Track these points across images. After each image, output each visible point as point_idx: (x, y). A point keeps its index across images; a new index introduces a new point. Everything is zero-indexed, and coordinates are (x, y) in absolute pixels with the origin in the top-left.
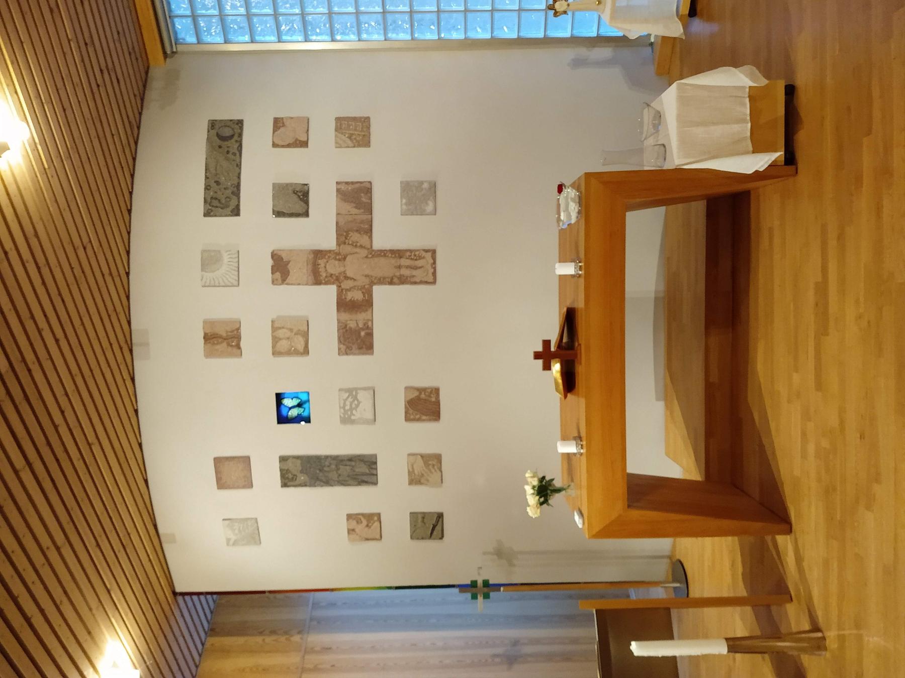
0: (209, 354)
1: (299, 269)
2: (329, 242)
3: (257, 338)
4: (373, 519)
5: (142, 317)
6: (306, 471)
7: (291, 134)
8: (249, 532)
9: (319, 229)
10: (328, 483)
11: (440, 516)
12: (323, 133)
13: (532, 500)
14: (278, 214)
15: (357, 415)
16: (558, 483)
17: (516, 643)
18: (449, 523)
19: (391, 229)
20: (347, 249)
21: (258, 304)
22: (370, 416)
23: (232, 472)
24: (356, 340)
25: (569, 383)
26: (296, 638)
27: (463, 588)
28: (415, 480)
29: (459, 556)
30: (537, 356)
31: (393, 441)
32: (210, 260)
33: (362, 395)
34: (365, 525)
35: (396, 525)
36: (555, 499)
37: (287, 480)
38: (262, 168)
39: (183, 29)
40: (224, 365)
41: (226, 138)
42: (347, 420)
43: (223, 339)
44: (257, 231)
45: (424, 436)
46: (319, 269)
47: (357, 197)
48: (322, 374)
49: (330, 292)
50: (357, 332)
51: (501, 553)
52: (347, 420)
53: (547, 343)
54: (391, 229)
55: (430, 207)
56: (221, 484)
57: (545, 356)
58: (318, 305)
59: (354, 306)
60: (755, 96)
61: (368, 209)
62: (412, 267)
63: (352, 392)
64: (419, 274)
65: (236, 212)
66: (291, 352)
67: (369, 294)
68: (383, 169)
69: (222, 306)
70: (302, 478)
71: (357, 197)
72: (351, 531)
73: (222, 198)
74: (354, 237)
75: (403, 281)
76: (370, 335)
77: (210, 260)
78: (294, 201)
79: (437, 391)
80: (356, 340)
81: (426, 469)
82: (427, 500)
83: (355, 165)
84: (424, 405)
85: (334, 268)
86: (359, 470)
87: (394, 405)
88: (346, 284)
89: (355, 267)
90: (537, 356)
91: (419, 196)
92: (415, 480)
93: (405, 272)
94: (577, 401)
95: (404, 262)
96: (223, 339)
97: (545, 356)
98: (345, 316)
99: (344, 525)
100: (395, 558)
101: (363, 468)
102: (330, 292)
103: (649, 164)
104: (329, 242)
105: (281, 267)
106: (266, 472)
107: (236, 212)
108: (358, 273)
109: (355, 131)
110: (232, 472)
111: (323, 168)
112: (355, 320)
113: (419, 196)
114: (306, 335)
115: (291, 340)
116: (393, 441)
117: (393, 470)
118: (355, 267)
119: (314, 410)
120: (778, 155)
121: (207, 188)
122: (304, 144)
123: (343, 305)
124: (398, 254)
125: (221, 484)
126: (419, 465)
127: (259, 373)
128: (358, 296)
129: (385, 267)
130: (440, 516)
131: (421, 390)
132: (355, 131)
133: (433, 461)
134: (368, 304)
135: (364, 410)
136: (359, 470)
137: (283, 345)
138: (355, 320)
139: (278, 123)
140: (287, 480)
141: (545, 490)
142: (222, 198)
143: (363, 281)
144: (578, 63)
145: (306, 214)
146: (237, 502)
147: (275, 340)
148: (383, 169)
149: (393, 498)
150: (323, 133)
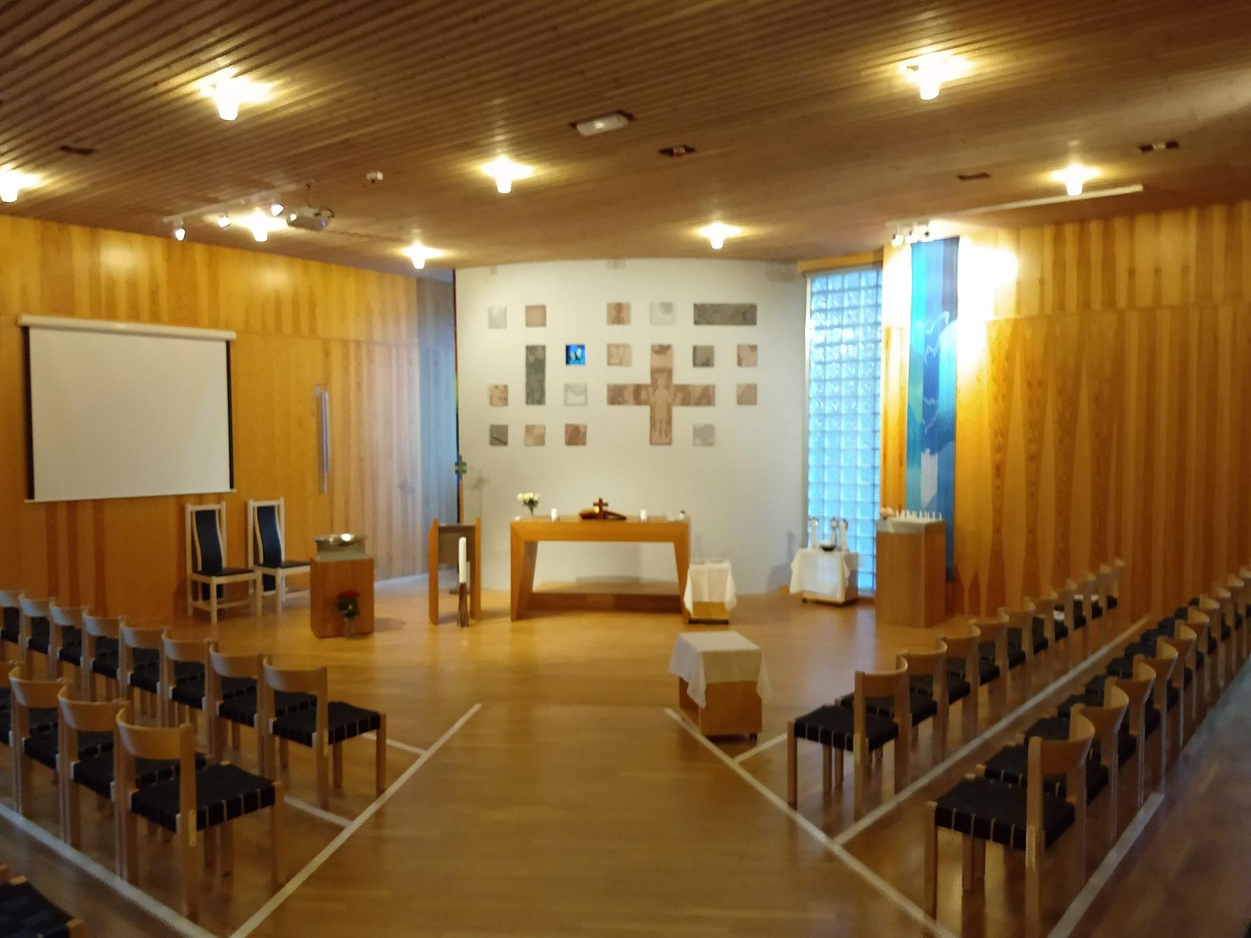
0: (609, 306)
1: (661, 361)
2: (678, 379)
3: (618, 334)
4: (504, 401)
5: (632, 265)
6: (536, 363)
7: (747, 355)
8: (497, 322)
9: (685, 373)
10: (528, 374)
11: (505, 443)
12: (747, 375)
13: (528, 496)
14: (695, 349)
15: (570, 394)
16: (535, 510)
17: (413, 491)
18: (500, 449)
19: (685, 418)
20: (673, 390)
21: (640, 335)
22: (570, 401)
23: (536, 316)
24: (616, 395)
25: (587, 516)
26: (416, 340)
27: (459, 457)
28: (529, 429)
29: (479, 454)
30: (601, 501)
31: (553, 416)
32: (667, 308)
33: (582, 398)
34: (500, 396)
35: (500, 416)
36: (527, 509)
37: (531, 349)
38: (726, 338)
39: (816, 285)
40: (603, 314)
41: (745, 315)
42: (568, 388)
43: (618, 314)
44: (685, 335)
45: (556, 436)
46: (662, 373)
47: (706, 397)
48: (596, 374)
49: (645, 379)
50: (621, 395)
51: (480, 482)
52: (568, 388)
53: (606, 505)
54: (685, 418)
55: (698, 441)
56: (529, 309)
57: (601, 504)
58: (639, 372)
59: (638, 394)
60: (721, 605)
61: (698, 403)
62: (661, 430)
63: (584, 391)
64: (656, 434)
65: (696, 323)
66: (610, 356)
67: (645, 403)
68: (723, 413)
69: (639, 312)
70: (532, 359)
71: (706, 397)
72: (497, 387)
73: (705, 314)
74: (680, 396)
75: (653, 424)
76: (620, 403)
77: (667, 308)
78: (703, 358)
79: (584, 443)
80: (616, 395)
81: (536, 436)
82: (516, 435)
83: (726, 395)
84: (575, 436)
85: (661, 381)
86: (536, 394)
87: (576, 417)
88: (651, 390)
89: (661, 395)
90: (601, 501)
91: (705, 436)
92: (529, 429)
93: (658, 427)
94: (578, 519)
95: (664, 425)
96: (618, 314)
97: (601, 504)
98: (631, 389)
99: (500, 382)
100: (478, 416)
101: (537, 396)
102: (645, 379)
103: (692, 559)
104: (678, 379)
105: (662, 350)
106: (536, 336)
107: (696, 323)
108: (659, 398)
109: (747, 396)
110: (536, 316)
111: (724, 377)
112: (629, 395)
113: (705, 436)
114: (620, 364)
115: (617, 354)
116: (553, 416)
117: (535, 414)
118: (661, 395)
119: (574, 368)
120: (693, 616)
121: (712, 306)
122: (740, 363)
123: (638, 389)
124: (669, 422)
125: (529, 309)
126: (538, 432)
127: (598, 336)
128: (644, 396)
129: (661, 414)
130: (505, 443)
131: (585, 434)
132: (747, 396)
133: (540, 440)
134: (638, 401)
135: (572, 398)
136: (536, 394)
137: (614, 350)
138: (629, 395)
139: (753, 348)
140: (531, 349)
141: (531, 503)
142: (705, 314)
143: (652, 400)
144: (791, 537)
145: (695, 364)
146: (517, 317)
147: (617, 346)
148: (723, 413)
149: (518, 414)
150: (747, 375)
